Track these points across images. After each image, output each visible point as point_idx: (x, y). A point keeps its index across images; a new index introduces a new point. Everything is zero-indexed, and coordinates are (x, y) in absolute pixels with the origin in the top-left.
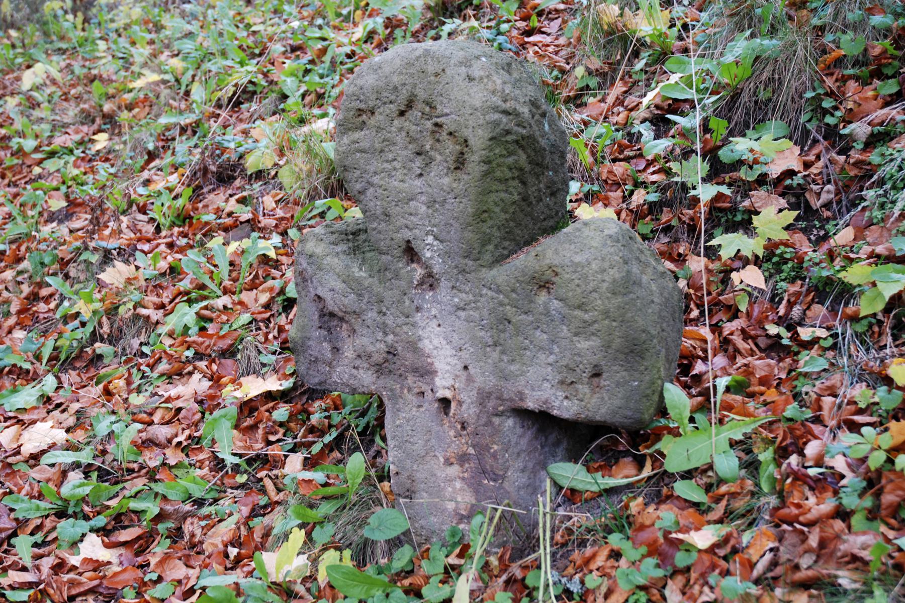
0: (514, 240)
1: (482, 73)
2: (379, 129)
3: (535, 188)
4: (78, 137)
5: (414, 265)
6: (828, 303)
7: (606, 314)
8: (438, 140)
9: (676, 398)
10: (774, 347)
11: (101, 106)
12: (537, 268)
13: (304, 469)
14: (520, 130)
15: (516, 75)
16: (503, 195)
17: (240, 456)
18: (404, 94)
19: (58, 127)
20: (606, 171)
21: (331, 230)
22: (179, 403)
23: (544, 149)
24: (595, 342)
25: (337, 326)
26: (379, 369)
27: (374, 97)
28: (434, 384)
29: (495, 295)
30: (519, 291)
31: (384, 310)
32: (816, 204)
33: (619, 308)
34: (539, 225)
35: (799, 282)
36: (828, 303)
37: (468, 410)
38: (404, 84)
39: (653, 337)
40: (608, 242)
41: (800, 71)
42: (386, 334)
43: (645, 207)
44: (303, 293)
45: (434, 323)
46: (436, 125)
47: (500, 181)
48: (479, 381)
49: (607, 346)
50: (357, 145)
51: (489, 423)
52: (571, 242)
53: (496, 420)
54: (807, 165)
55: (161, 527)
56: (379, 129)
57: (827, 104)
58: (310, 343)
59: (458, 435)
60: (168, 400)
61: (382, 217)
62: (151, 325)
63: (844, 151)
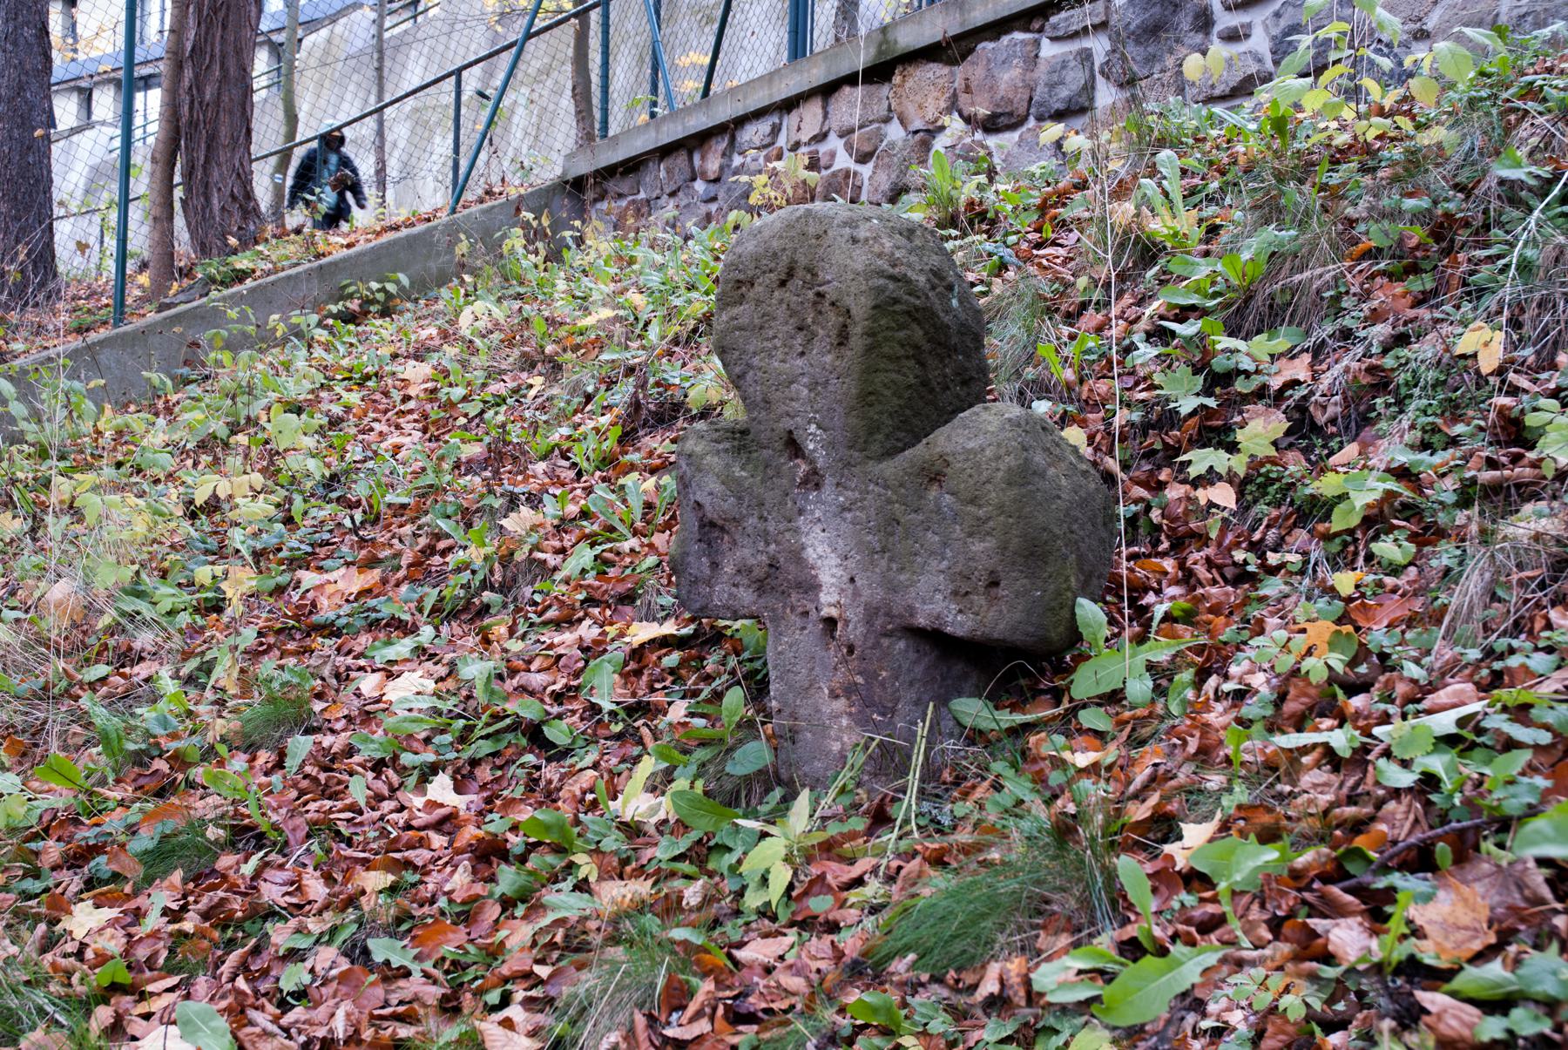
2: (758, 302)
4: (513, 385)
5: (798, 461)
7: (1001, 508)
10: (1242, 577)
14: (912, 300)
15: (918, 242)
16: (894, 376)
17: (618, 703)
18: (785, 260)
19: (494, 374)
22: (561, 651)
23: (948, 327)
24: (990, 543)
27: (753, 265)
30: (908, 485)
33: (1015, 501)
37: (854, 631)
39: (1057, 537)
45: (817, 529)
47: (889, 358)
49: (1003, 548)
51: (877, 645)
52: (965, 427)
53: (885, 642)
56: (758, 302)
60: (551, 647)
62: (548, 571)
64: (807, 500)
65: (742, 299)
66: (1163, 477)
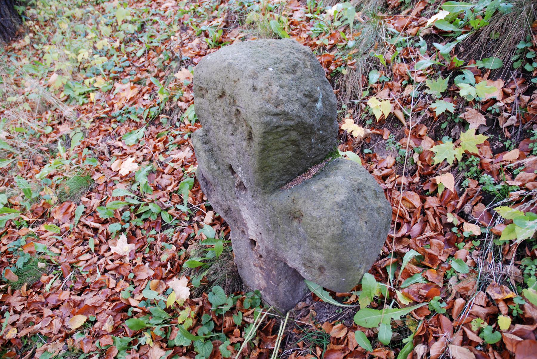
12: (293, 208)
16: (280, 155)
32: (503, 125)
33: (335, 249)
40: (335, 207)
54: (506, 95)
64: (240, 194)
66: (421, 133)
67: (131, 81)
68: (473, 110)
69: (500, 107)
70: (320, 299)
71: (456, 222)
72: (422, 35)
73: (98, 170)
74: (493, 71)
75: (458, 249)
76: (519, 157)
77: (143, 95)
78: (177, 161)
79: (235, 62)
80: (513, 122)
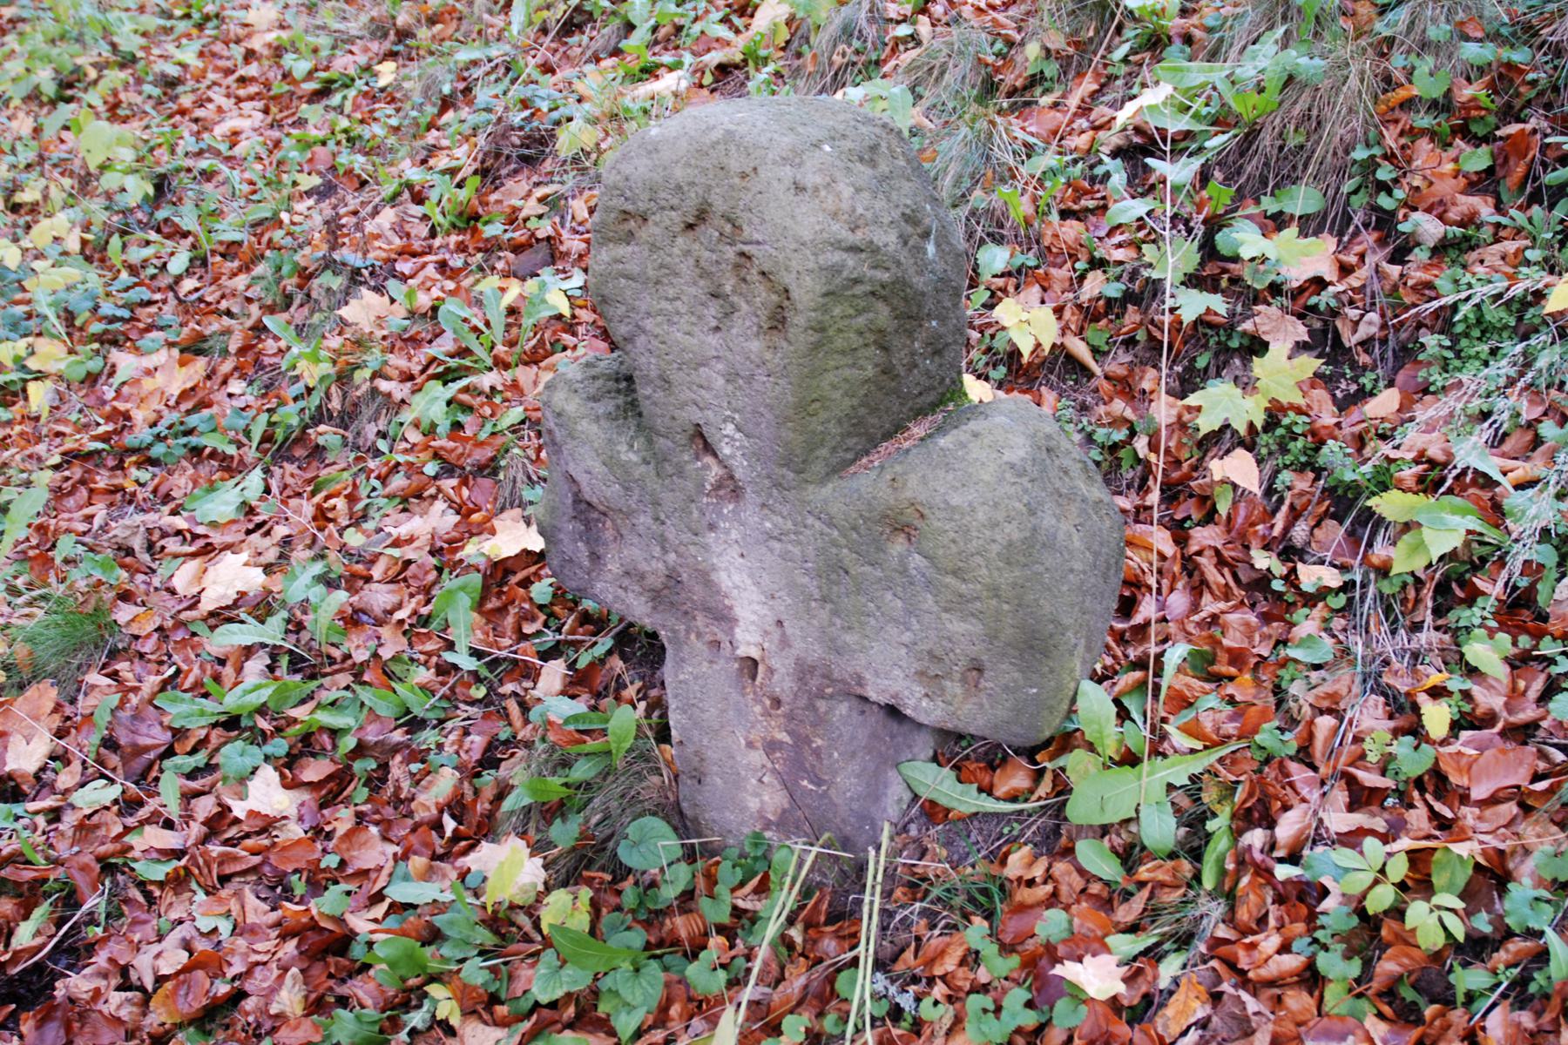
0: (866, 433)
1: (818, 179)
2: (654, 248)
3: (906, 351)
6: (1348, 523)
8: (744, 280)
9: (1095, 707)
11: (394, 18)
12: (892, 502)
13: (563, 693)
15: (884, 168)
16: (847, 372)
18: (692, 200)
20: (1049, 233)
21: (593, 372)
24: (974, 627)
25: (598, 520)
26: (656, 596)
28: (733, 635)
29: (827, 530)
30: (863, 530)
31: (663, 517)
32: (1350, 340)
33: (1014, 585)
34: (910, 404)
35: (1311, 475)
36: (1348, 523)
37: (783, 684)
38: (692, 184)
40: (1008, 475)
41: (1350, 110)
42: (665, 550)
43: (1101, 303)
44: (554, 458)
46: (742, 254)
47: (843, 353)
48: (798, 646)
50: (621, 266)
52: (948, 467)
53: (822, 705)
54: (1345, 270)
55: (358, 766)
56: (654, 248)
57: (1385, 173)
58: (562, 536)
59: (766, 714)
61: (659, 383)
63: (1398, 257)
64: (719, 514)
65: (630, 237)
67: (171, 345)
68: (1273, 310)
69: (1337, 296)
70: (948, 811)
71: (1279, 569)
72: (1106, 150)
73: (126, 596)
74: (1304, 220)
75: (1292, 625)
76: (1401, 405)
77: (225, 382)
78: (411, 540)
79: (743, 129)
80: (1374, 330)
